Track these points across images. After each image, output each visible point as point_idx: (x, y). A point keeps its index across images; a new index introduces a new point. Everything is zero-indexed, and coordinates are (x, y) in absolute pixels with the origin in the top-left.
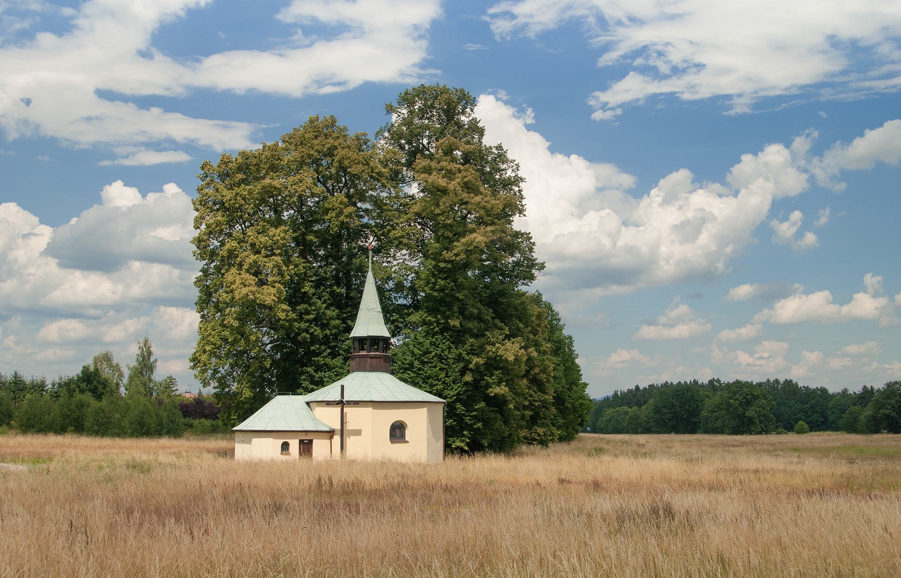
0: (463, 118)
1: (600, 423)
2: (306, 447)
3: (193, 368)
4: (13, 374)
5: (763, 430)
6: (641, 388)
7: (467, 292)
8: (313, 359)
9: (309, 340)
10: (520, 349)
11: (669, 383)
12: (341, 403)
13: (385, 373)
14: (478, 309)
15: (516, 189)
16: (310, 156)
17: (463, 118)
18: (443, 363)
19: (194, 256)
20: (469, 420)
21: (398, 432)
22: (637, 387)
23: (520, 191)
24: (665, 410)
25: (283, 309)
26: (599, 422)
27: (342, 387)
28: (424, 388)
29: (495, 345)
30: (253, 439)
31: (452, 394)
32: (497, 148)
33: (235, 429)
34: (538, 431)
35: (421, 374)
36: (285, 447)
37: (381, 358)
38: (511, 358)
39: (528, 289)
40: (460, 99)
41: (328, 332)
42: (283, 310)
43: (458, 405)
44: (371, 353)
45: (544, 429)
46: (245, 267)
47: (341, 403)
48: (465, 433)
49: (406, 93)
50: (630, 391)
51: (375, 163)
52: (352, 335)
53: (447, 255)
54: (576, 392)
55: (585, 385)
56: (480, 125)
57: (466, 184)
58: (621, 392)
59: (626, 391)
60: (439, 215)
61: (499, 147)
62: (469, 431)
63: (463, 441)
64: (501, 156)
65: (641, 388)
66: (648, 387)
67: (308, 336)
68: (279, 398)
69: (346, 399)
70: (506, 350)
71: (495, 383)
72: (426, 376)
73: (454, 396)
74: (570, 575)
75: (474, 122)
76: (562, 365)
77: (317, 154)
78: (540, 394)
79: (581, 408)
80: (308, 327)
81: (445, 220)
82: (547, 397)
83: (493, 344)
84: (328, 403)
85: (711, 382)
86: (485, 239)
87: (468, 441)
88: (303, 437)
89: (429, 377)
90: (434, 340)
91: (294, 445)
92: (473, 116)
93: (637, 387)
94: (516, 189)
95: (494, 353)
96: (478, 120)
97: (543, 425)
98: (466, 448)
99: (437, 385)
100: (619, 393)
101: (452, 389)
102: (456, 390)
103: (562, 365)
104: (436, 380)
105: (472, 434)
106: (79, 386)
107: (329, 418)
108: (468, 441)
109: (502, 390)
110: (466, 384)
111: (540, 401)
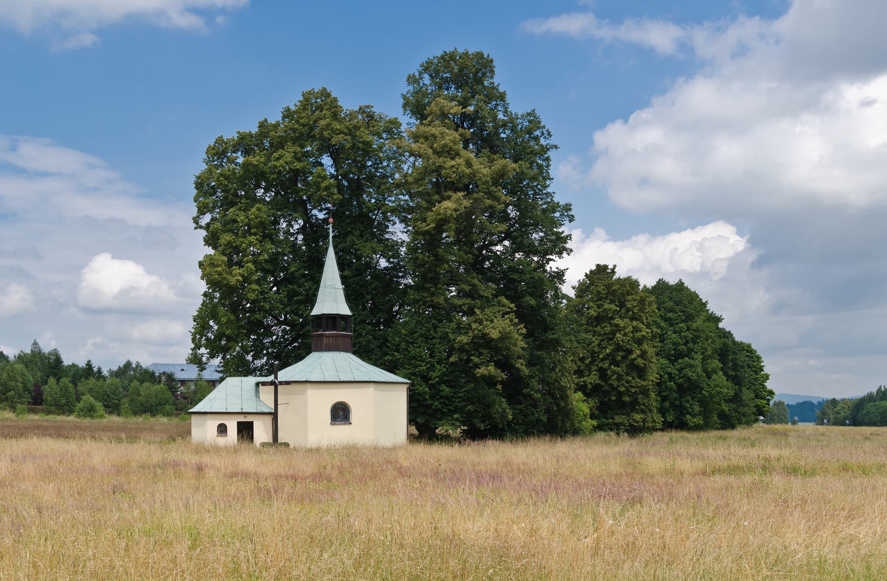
1: (859, 417)
2: (246, 430)
3: (763, 366)
12: (272, 383)
13: (342, 353)
18: (429, 343)
20: (459, 402)
21: (340, 413)
25: (252, 290)
26: (859, 415)
30: (208, 421)
33: (189, 411)
36: (222, 429)
37: (338, 336)
44: (327, 332)
48: (456, 416)
52: (317, 311)
54: (714, 380)
55: (767, 377)
61: (532, 114)
72: (410, 357)
73: (437, 377)
80: (297, 308)
88: (242, 419)
89: (415, 358)
91: (232, 429)
95: (480, 331)
99: (421, 366)
100: (883, 389)
104: (420, 361)
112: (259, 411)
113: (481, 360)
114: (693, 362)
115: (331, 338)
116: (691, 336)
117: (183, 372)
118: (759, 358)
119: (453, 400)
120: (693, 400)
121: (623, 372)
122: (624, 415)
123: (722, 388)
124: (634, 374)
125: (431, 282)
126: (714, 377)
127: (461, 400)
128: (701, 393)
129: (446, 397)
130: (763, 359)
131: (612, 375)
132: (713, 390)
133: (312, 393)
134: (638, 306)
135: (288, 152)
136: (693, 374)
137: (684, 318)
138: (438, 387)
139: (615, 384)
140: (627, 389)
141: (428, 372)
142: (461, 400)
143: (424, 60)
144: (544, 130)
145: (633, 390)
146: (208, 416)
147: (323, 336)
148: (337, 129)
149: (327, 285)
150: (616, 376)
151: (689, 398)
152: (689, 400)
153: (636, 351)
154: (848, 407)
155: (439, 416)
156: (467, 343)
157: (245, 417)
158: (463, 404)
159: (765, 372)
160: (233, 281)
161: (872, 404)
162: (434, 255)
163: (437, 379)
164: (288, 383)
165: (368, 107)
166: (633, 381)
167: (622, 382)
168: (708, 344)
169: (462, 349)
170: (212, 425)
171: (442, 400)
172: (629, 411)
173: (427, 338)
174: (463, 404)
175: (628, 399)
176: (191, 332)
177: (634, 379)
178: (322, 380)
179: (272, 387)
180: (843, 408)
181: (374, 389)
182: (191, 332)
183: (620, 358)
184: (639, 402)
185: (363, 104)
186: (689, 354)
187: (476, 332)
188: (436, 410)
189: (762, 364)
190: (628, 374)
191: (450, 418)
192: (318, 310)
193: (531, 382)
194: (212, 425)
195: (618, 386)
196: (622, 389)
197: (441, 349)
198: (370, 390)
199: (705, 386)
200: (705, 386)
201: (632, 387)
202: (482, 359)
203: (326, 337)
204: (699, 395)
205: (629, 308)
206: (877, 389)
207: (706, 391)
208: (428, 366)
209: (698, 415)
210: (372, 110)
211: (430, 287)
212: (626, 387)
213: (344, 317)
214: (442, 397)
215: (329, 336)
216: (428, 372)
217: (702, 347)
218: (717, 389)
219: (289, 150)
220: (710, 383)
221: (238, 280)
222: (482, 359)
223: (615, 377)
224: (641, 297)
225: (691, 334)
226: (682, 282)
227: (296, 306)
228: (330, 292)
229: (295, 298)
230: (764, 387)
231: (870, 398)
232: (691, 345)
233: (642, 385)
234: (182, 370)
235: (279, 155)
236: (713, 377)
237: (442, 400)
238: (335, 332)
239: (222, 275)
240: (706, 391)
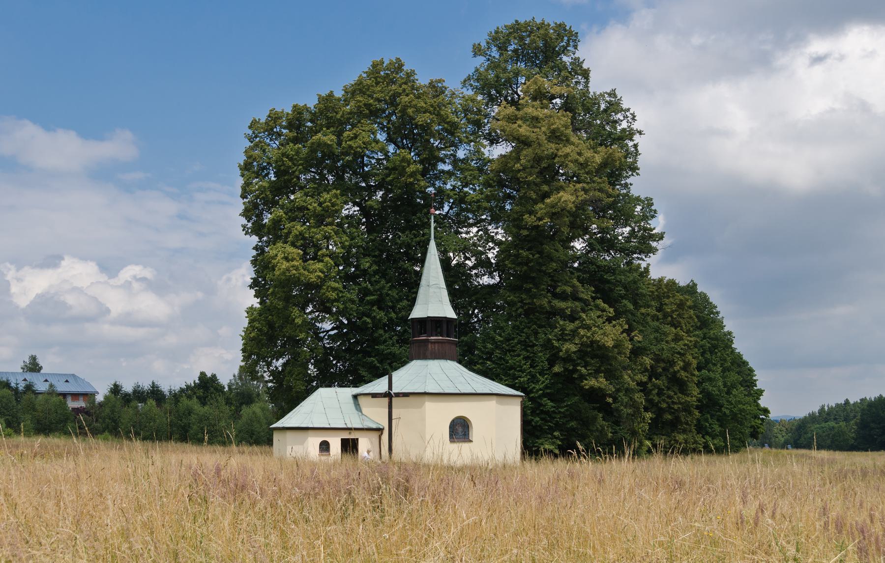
0: (565, 59)
2: (350, 446)
3: (755, 381)
4: (151, 384)
6: (852, 402)
7: (555, 265)
8: (376, 347)
9: (370, 325)
10: (622, 333)
12: (388, 395)
14: (573, 286)
15: (630, 144)
16: (368, 106)
17: (565, 59)
18: (528, 351)
19: (243, 230)
22: (847, 402)
23: (636, 146)
24: (872, 425)
25: (332, 288)
28: (505, 381)
29: (591, 328)
30: (309, 438)
31: (537, 387)
32: (610, 95)
34: (677, 438)
35: (502, 364)
36: (325, 447)
37: (444, 342)
38: (610, 343)
40: (560, 37)
41: (393, 315)
42: (334, 289)
43: (545, 400)
44: (432, 338)
45: (685, 436)
46: (290, 239)
48: (556, 434)
49: (497, 32)
51: (448, 111)
53: (529, 219)
54: (735, 396)
55: (760, 392)
56: (585, 66)
57: (553, 132)
58: (828, 406)
59: (834, 406)
60: (519, 171)
61: (613, 94)
62: (561, 431)
63: (553, 443)
64: (615, 106)
65: (852, 402)
66: (859, 401)
67: (368, 320)
68: (321, 391)
69: (395, 390)
70: (604, 334)
71: (591, 374)
73: (541, 390)
74: (25, 562)
75: (577, 63)
76: (719, 366)
77: (376, 103)
78: (680, 395)
79: (741, 414)
80: (370, 310)
81: (526, 177)
82: (689, 399)
83: (588, 328)
84: (374, 395)
86: (573, 198)
87: (560, 443)
88: (346, 435)
89: (511, 368)
90: (518, 323)
92: (577, 55)
93: (847, 402)
94: (630, 144)
95: (588, 338)
96: (581, 60)
97: (684, 431)
98: (557, 451)
99: (520, 377)
100: (826, 408)
101: (538, 382)
102: (543, 382)
103: (719, 366)
104: (519, 371)
105: (565, 435)
106: (195, 393)
107: (376, 413)
108: (560, 443)
109: (600, 382)
110: (557, 375)
111: (680, 403)
112: (365, 427)
113: (588, 370)
114: (712, 375)
115: (436, 345)
116: (708, 345)
117: (67, 383)
118: (751, 370)
119: (554, 415)
120: (711, 419)
121: (664, 385)
122: (664, 435)
123: (744, 405)
124: (676, 389)
125: (530, 283)
126: (734, 392)
127: (562, 415)
128: (720, 410)
129: (547, 413)
130: (755, 373)
131: (653, 390)
132: (735, 407)
133: (431, 407)
134: (676, 311)
135: (363, 131)
136: (714, 389)
137: (699, 324)
138: (539, 401)
139: (656, 399)
140: (669, 405)
141: (528, 383)
142: (562, 415)
143: (493, 29)
144: (628, 113)
145: (676, 407)
146: (310, 432)
147: (429, 342)
148: (422, 107)
149: (431, 284)
150: (657, 390)
151: (709, 416)
152: (708, 419)
153: (679, 362)
154: (787, 429)
155: (538, 433)
156: (574, 353)
157: (350, 433)
158: (564, 420)
159: (758, 387)
160: (313, 278)
161: (818, 426)
162: (539, 253)
163: (541, 392)
164: (406, 395)
165: (440, 81)
166: (675, 396)
167: (663, 398)
168: (727, 355)
169: (567, 359)
170: (313, 443)
171: (543, 416)
172: (669, 431)
173: (526, 345)
174: (564, 420)
175: (669, 417)
176: (242, 336)
177: (676, 394)
178: (442, 391)
179: (386, 400)
180: (780, 431)
181: (497, 403)
182: (242, 336)
183: (661, 370)
184: (681, 421)
185: (435, 78)
186: (706, 366)
187: (585, 339)
188: (535, 427)
189: (754, 378)
190: (668, 389)
191: (550, 436)
192: (418, 312)
193: (619, 396)
194: (313, 443)
195: (659, 402)
196: (664, 405)
197: (543, 357)
198: (492, 403)
199: (726, 403)
200: (726, 403)
201: (674, 403)
202: (589, 370)
203: (432, 343)
204: (718, 413)
205: (667, 312)
206: (819, 408)
207: (727, 408)
208: (529, 377)
209: (718, 436)
210: (444, 84)
211: (530, 288)
212: (667, 403)
213: (448, 320)
214: (542, 412)
215: (434, 343)
216: (528, 383)
217: (720, 357)
218: (739, 406)
219: (363, 128)
220: (730, 399)
221: (319, 277)
222: (589, 370)
223: (656, 391)
224: (681, 300)
225: (709, 343)
226: (693, 283)
227: (368, 307)
228: (435, 292)
229: (368, 298)
230: (758, 405)
231: (812, 418)
232: (708, 356)
233: (686, 400)
234: (67, 381)
235: (355, 134)
236: (733, 393)
237: (543, 416)
238: (441, 338)
239: (299, 270)
240: (727, 408)
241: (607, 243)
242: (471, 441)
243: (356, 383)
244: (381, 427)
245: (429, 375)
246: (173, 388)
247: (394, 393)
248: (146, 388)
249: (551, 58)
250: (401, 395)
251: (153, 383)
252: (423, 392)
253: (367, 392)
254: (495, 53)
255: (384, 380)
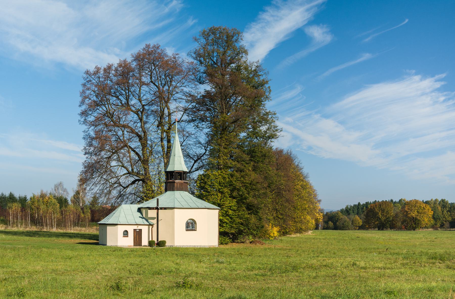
5: (143, 199)
6: (361, 204)
11: (377, 201)
22: (359, 203)
27: (158, 200)
36: (126, 234)
39: (275, 144)
47: (157, 208)
50: (355, 205)
58: (350, 206)
65: (361, 204)
69: (159, 207)
85: (400, 201)
88: (135, 227)
93: (359, 203)
100: (349, 207)
164: (165, 209)
179: (156, 211)
206: (345, 207)
238: (180, 181)
241: (255, 134)
242: (128, 236)
243: (139, 202)
244: (153, 224)
245: (175, 199)
246: (21, 196)
247: (160, 208)
248: (7, 195)
249: (267, 96)
250: (163, 209)
251: (11, 193)
252: (173, 207)
253: (146, 207)
254: (203, 41)
255: (154, 201)
